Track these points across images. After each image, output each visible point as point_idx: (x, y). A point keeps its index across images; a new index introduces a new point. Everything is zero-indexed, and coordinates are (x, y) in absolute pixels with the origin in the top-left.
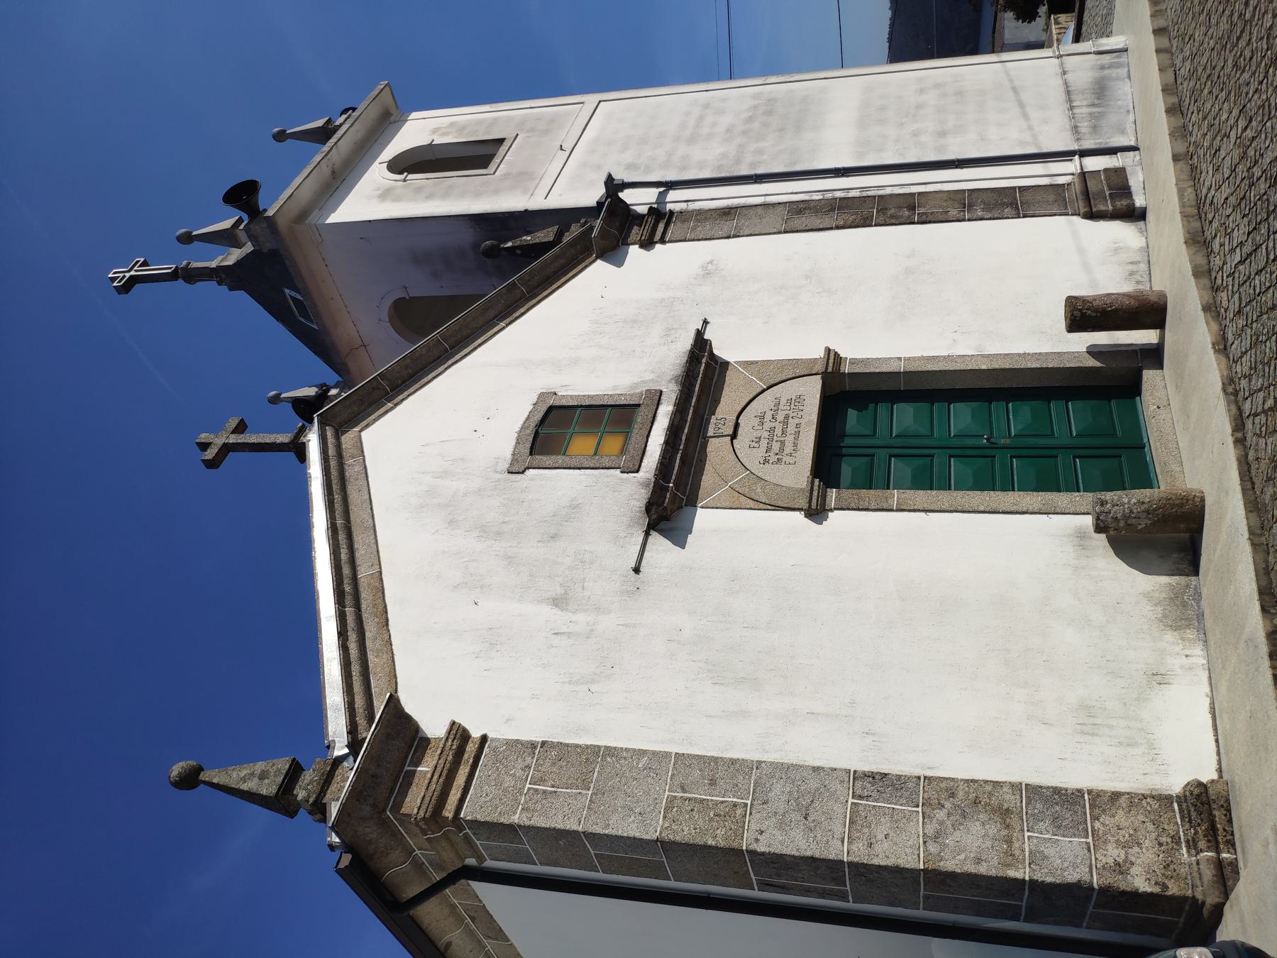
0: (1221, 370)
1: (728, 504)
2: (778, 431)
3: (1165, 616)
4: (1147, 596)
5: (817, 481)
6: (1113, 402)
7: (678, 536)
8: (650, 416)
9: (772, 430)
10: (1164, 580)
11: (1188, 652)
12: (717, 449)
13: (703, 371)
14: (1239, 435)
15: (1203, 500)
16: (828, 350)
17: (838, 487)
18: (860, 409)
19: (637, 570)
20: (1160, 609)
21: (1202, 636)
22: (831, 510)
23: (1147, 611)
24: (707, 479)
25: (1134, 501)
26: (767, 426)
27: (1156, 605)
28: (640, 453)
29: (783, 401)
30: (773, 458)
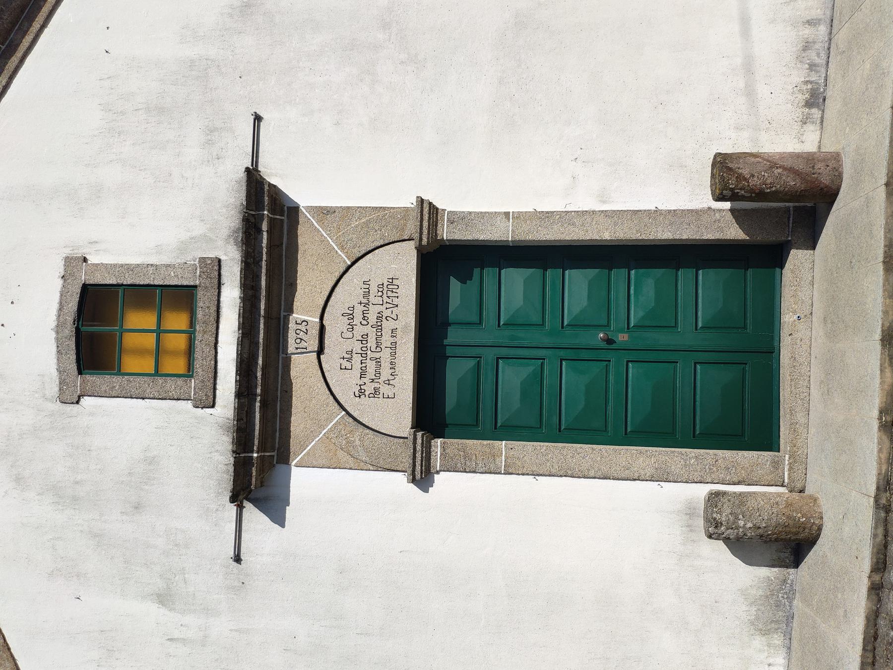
0: (880, 464)
3: (757, 618)
4: (743, 592)
6: (750, 272)
7: (274, 505)
9: (364, 338)
10: (764, 572)
11: (771, 661)
12: (302, 367)
13: (268, 221)
14: (877, 578)
15: (820, 529)
16: (421, 201)
18: (464, 278)
19: (238, 559)
20: (754, 609)
21: (787, 641)
22: (438, 472)
23: (743, 611)
24: (298, 424)
25: (749, 525)
26: (359, 331)
27: (751, 604)
28: (211, 375)
29: (374, 289)
30: (369, 389)
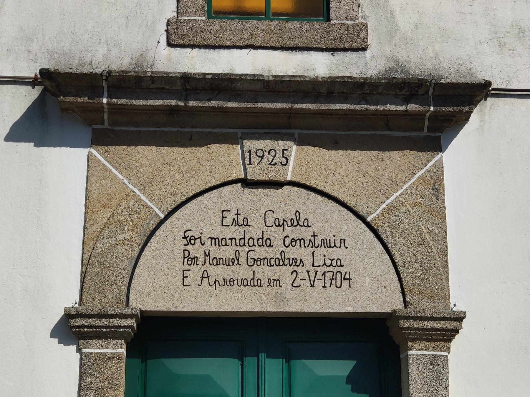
1: (95, 191)
2: (259, 252)
5: (133, 322)
8: (300, 43)
16: (459, 318)
17: (130, 354)
22: (79, 350)
26: (276, 235)
28: (211, 42)
30: (196, 250)
